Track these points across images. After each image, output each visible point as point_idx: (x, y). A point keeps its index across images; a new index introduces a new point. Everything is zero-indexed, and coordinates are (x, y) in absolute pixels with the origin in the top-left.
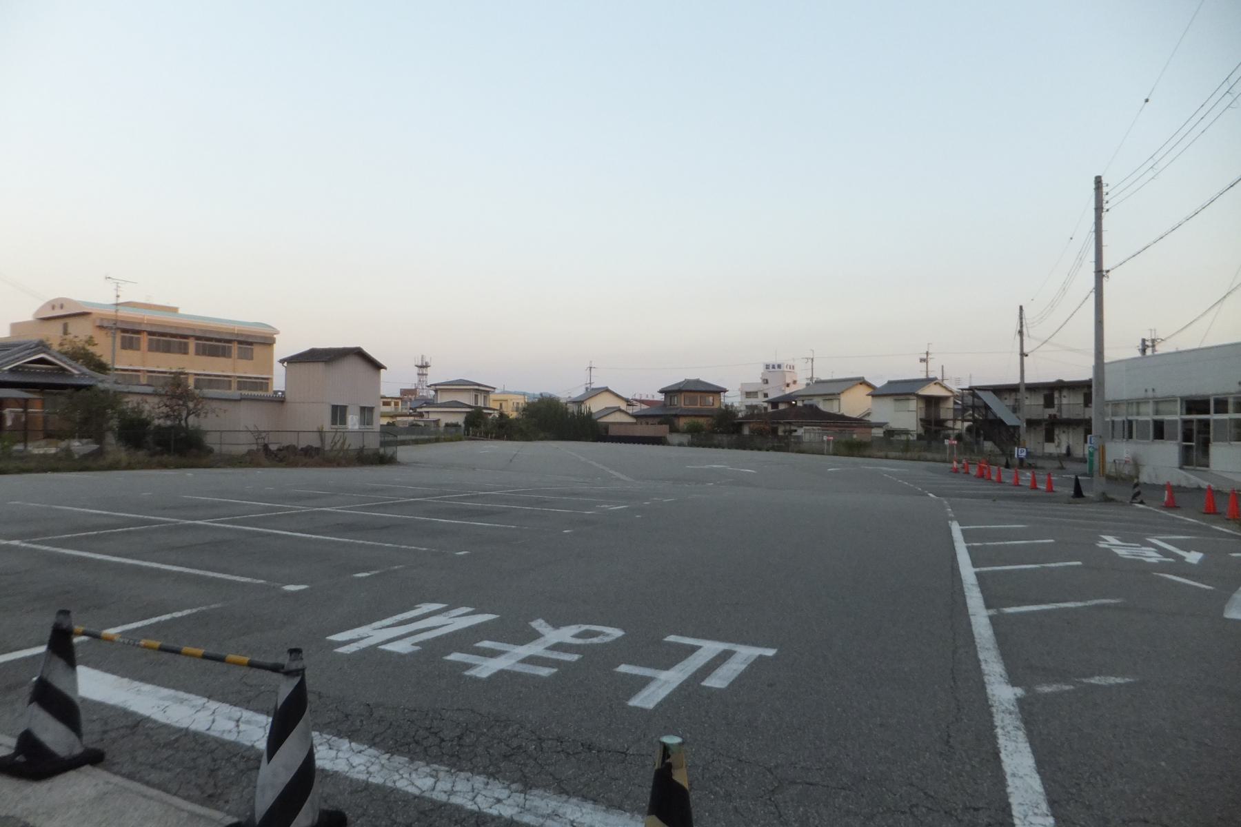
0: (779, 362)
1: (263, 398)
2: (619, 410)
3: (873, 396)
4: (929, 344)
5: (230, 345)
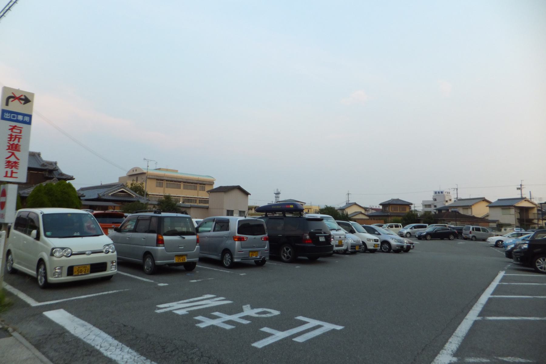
0: (442, 190)
1: (194, 206)
2: (361, 213)
3: (490, 207)
4: (521, 181)
5: (180, 183)
